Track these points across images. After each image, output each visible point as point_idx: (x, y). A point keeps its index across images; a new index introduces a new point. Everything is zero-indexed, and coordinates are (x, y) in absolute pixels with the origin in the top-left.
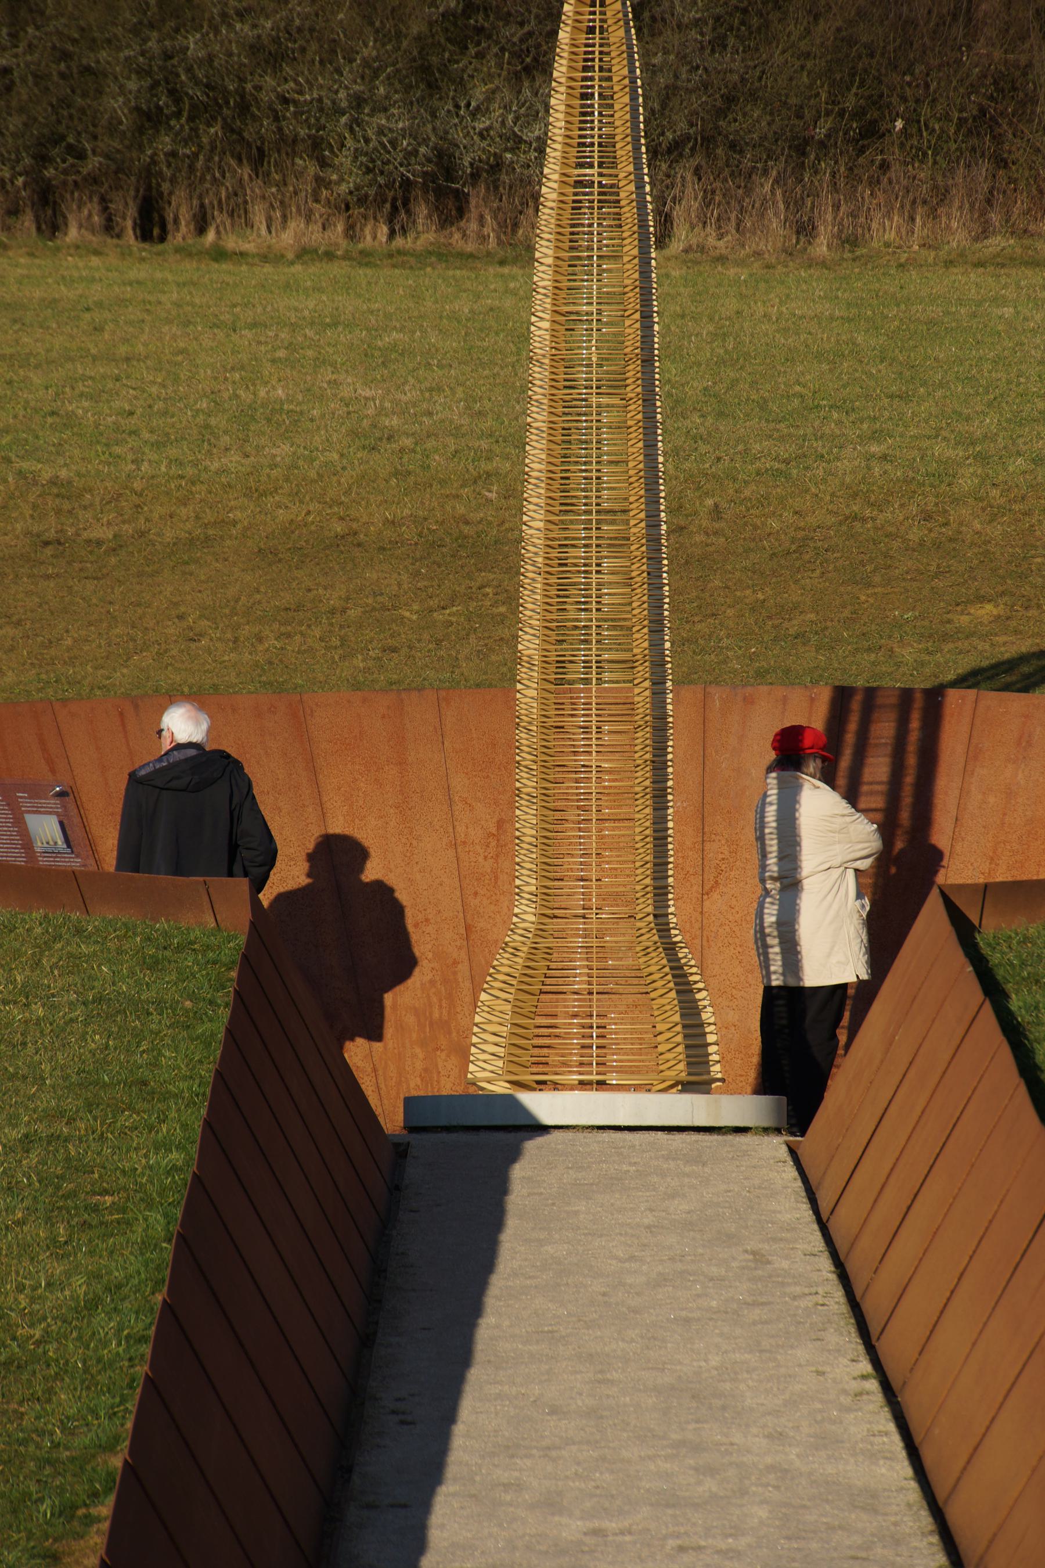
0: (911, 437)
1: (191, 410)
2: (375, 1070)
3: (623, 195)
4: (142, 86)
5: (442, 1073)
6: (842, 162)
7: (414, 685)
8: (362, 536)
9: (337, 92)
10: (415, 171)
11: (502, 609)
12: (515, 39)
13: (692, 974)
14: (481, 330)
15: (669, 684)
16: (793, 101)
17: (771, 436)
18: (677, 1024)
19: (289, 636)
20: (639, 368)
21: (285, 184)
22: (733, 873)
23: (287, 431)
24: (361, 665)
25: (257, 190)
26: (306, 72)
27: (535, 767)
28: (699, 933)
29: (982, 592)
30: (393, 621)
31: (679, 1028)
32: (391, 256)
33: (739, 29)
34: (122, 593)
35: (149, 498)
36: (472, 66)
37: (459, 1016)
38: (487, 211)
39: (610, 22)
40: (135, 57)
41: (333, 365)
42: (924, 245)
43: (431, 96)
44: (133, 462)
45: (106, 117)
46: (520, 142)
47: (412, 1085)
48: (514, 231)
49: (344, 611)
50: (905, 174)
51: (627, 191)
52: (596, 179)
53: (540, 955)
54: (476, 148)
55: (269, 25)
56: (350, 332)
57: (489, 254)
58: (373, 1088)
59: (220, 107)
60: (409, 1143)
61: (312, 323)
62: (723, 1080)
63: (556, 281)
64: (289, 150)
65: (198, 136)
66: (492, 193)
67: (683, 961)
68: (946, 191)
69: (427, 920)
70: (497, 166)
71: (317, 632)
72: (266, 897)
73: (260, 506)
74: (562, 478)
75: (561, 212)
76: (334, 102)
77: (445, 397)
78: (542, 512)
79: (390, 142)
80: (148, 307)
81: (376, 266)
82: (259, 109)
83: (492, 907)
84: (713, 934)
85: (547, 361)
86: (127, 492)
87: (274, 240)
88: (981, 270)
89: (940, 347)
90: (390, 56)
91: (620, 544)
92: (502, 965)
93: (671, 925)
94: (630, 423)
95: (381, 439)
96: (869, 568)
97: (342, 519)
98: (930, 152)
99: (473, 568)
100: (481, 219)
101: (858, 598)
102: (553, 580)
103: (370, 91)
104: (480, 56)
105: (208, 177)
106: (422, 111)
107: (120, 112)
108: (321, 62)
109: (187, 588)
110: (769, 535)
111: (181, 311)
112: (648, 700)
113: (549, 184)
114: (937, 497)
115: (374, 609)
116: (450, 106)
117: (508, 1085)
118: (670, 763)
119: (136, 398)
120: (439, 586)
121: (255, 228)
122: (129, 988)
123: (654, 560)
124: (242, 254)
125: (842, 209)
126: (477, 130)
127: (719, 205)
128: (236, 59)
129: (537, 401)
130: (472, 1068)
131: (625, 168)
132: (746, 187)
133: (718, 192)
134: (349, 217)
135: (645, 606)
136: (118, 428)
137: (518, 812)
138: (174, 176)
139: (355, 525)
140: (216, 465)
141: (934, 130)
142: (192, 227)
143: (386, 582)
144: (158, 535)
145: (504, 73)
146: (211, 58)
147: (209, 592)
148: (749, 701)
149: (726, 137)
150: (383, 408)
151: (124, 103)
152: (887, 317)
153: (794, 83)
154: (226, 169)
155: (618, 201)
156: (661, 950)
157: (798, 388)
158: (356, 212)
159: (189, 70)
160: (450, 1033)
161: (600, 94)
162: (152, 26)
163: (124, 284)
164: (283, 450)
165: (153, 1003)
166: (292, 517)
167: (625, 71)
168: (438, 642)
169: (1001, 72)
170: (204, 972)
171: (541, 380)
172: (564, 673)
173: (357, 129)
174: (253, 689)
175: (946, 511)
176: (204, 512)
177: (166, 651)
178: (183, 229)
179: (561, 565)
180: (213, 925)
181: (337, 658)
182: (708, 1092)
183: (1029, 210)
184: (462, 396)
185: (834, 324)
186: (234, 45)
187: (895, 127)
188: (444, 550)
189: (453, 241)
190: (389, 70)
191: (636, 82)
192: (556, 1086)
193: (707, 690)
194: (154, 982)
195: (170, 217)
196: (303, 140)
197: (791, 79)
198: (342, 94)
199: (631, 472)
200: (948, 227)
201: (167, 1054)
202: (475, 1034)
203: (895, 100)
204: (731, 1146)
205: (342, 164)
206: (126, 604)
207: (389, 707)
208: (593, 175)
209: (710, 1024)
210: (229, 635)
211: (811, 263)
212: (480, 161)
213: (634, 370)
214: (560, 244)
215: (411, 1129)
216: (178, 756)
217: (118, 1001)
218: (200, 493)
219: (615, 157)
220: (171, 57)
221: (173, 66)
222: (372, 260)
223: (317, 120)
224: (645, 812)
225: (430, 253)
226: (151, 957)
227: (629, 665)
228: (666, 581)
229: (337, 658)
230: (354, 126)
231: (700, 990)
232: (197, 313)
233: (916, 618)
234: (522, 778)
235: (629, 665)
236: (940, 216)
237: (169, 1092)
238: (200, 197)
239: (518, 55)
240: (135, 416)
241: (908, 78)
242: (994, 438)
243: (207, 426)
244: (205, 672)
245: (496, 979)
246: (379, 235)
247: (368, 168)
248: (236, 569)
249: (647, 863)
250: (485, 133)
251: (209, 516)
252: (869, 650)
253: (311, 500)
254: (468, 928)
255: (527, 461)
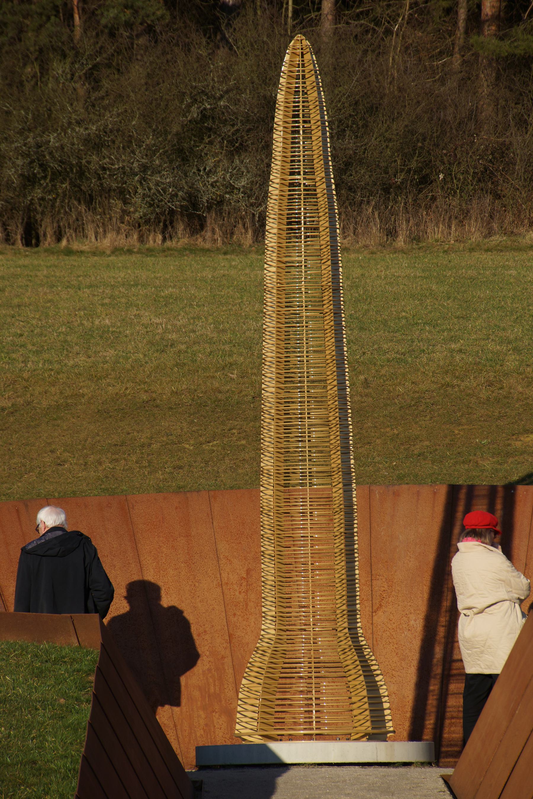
0: (473, 339)
1: (56, 333)
2: (175, 726)
3: (318, 191)
4: (24, 163)
5: (217, 726)
6: (410, 197)
7: (193, 488)
8: (158, 401)
9: (133, 163)
10: (175, 205)
11: (243, 442)
12: (230, 134)
13: (372, 665)
14: (219, 286)
15: (354, 485)
16: (383, 164)
17: (392, 340)
18: (365, 697)
19: (117, 460)
20: (331, 294)
21: (105, 214)
22: (390, 599)
23: (112, 343)
24: (161, 477)
25: (89, 218)
26: (116, 153)
27: (273, 538)
28: (371, 636)
29: (527, 428)
30: (180, 450)
31: (366, 700)
32: (164, 251)
33: (352, 127)
34: (17, 438)
35: (33, 383)
36: (207, 149)
37: (226, 691)
38: (216, 226)
39: (308, 88)
40: (21, 147)
41: (137, 306)
42: (457, 240)
43: (184, 165)
44: (22, 362)
45: (5, 180)
46: (233, 189)
47: (198, 735)
48: (231, 237)
49: (150, 445)
50: (445, 203)
51: (321, 188)
52: (302, 182)
53: (279, 655)
54: (210, 192)
55: (94, 128)
56: (145, 289)
57: (218, 249)
58: (174, 737)
59: (68, 173)
60: (202, 781)
61: (124, 285)
62: (394, 732)
63: (279, 243)
64: (107, 195)
65: (56, 189)
66: (219, 216)
67: (367, 657)
68: (468, 211)
69: (205, 631)
70: (221, 202)
71: (134, 458)
72: (105, 621)
73: (98, 385)
74: (285, 361)
75: (281, 202)
76: (131, 169)
77: (202, 322)
78: (274, 382)
79: (162, 189)
80: (30, 278)
81: (156, 256)
82: (89, 174)
83: (245, 622)
84: (379, 637)
85: (275, 291)
86: (20, 379)
87: (99, 244)
88: (489, 253)
89: (480, 291)
90: (161, 144)
91: (321, 401)
92: (256, 661)
93: (359, 635)
94: (326, 327)
95: (167, 346)
96: (459, 414)
97: (146, 391)
98: (458, 191)
99: (225, 419)
100: (213, 231)
101: (454, 432)
102: (282, 423)
103: (151, 163)
104: (211, 143)
105: (62, 211)
106: (180, 173)
107: (13, 177)
108: (123, 148)
109: (56, 434)
110: (398, 396)
111: (49, 280)
112: (341, 495)
113: (274, 185)
114: (495, 372)
115: (167, 444)
116: (195, 170)
117: (260, 737)
118: (356, 534)
119: (24, 327)
120: (205, 429)
121: (89, 238)
122: (23, 692)
123: (343, 409)
124: (82, 252)
125: (411, 222)
126: (210, 183)
127: (343, 221)
128: (76, 147)
129: (269, 315)
130: (238, 727)
131: (320, 175)
132: (358, 211)
133: (343, 214)
134: (140, 231)
135: (338, 438)
136: (14, 344)
137: (263, 566)
138: (43, 211)
139: (154, 395)
140: (71, 363)
141: (460, 179)
142: (54, 238)
143: (174, 427)
144: (38, 403)
145: (224, 152)
146: (62, 147)
147: (69, 436)
148: (396, 494)
149: (347, 184)
150: (167, 329)
151: (15, 172)
152: (446, 276)
153: (383, 154)
154: (72, 207)
155: (316, 195)
156: (353, 650)
157: (404, 314)
158: (144, 228)
159: (51, 153)
160: (221, 701)
161: (303, 131)
162: (29, 130)
163: (17, 267)
164: (111, 353)
165: (39, 701)
166: (117, 391)
167: (318, 117)
168: (207, 463)
169: (495, 148)
170: (72, 678)
171: (271, 302)
172: (289, 480)
173: (144, 183)
174: (97, 493)
175: (501, 381)
176: (65, 390)
177: (44, 472)
178: (49, 239)
179: (285, 414)
180: (77, 644)
181: (146, 473)
182: (385, 741)
183: (513, 222)
184: (212, 321)
185: (418, 280)
186: (75, 139)
187: (439, 178)
188: (207, 408)
189: (198, 242)
190: (161, 151)
191: (325, 124)
192: (291, 738)
193: (371, 488)
194: (40, 686)
195: (41, 233)
196: (114, 190)
197: (381, 153)
198: (135, 165)
199: (328, 357)
200: (470, 231)
201: (49, 739)
202: (239, 705)
203: (438, 163)
204: (407, 779)
205: (136, 202)
206: (20, 444)
207: (179, 502)
208: (300, 179)
209: (384, 696)
210: (81, 462)
211: (396, 250)
212: (212, 199)
213: (328, 295)
214: (281, 221)
215: (201, 767)
216: (51, 536)
217: (17, 701)
218: (62, 379)
219: (313, 168)
220: (40, 147)
221: (42, 151)
222: (154, 253)
223: (122, 178)
224: (341, 565)
225: (185, 249)
226: (38, 668)
227: (329, 474)
228: (350, 423)
229: (146, 473)
230: (142, 181)
231: (378, 675)
232: (58, 281)
233: (489, 443)
234: (265, 545)
235: (329, 474)
236: (465, 225)
237: (51, 769)
238: (58, 222)
239: (231, 142)
240: (24, 337)
241: (445, 151)
242: (521, 339)
243: (66, 341)
244: (68, 483)
245: (252, 670)
246: (157, 240)
247: (150, 203)
248: (85, 423)
249: (343, 596)
250: (214, 184)
251: (68, 392)
252: (463, 462)
253: (128, 381)
254: (230, 636)
255: (264, 351)
